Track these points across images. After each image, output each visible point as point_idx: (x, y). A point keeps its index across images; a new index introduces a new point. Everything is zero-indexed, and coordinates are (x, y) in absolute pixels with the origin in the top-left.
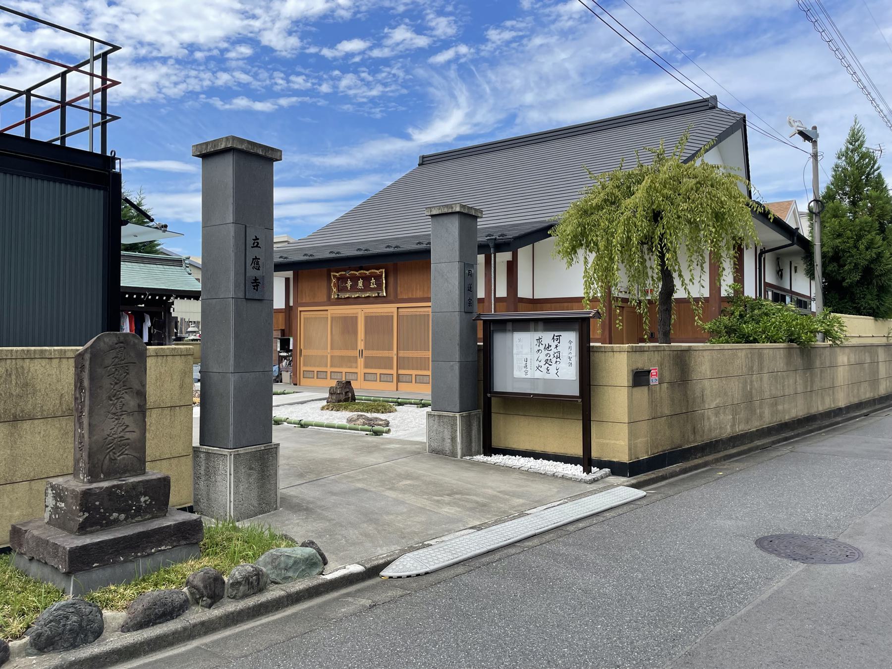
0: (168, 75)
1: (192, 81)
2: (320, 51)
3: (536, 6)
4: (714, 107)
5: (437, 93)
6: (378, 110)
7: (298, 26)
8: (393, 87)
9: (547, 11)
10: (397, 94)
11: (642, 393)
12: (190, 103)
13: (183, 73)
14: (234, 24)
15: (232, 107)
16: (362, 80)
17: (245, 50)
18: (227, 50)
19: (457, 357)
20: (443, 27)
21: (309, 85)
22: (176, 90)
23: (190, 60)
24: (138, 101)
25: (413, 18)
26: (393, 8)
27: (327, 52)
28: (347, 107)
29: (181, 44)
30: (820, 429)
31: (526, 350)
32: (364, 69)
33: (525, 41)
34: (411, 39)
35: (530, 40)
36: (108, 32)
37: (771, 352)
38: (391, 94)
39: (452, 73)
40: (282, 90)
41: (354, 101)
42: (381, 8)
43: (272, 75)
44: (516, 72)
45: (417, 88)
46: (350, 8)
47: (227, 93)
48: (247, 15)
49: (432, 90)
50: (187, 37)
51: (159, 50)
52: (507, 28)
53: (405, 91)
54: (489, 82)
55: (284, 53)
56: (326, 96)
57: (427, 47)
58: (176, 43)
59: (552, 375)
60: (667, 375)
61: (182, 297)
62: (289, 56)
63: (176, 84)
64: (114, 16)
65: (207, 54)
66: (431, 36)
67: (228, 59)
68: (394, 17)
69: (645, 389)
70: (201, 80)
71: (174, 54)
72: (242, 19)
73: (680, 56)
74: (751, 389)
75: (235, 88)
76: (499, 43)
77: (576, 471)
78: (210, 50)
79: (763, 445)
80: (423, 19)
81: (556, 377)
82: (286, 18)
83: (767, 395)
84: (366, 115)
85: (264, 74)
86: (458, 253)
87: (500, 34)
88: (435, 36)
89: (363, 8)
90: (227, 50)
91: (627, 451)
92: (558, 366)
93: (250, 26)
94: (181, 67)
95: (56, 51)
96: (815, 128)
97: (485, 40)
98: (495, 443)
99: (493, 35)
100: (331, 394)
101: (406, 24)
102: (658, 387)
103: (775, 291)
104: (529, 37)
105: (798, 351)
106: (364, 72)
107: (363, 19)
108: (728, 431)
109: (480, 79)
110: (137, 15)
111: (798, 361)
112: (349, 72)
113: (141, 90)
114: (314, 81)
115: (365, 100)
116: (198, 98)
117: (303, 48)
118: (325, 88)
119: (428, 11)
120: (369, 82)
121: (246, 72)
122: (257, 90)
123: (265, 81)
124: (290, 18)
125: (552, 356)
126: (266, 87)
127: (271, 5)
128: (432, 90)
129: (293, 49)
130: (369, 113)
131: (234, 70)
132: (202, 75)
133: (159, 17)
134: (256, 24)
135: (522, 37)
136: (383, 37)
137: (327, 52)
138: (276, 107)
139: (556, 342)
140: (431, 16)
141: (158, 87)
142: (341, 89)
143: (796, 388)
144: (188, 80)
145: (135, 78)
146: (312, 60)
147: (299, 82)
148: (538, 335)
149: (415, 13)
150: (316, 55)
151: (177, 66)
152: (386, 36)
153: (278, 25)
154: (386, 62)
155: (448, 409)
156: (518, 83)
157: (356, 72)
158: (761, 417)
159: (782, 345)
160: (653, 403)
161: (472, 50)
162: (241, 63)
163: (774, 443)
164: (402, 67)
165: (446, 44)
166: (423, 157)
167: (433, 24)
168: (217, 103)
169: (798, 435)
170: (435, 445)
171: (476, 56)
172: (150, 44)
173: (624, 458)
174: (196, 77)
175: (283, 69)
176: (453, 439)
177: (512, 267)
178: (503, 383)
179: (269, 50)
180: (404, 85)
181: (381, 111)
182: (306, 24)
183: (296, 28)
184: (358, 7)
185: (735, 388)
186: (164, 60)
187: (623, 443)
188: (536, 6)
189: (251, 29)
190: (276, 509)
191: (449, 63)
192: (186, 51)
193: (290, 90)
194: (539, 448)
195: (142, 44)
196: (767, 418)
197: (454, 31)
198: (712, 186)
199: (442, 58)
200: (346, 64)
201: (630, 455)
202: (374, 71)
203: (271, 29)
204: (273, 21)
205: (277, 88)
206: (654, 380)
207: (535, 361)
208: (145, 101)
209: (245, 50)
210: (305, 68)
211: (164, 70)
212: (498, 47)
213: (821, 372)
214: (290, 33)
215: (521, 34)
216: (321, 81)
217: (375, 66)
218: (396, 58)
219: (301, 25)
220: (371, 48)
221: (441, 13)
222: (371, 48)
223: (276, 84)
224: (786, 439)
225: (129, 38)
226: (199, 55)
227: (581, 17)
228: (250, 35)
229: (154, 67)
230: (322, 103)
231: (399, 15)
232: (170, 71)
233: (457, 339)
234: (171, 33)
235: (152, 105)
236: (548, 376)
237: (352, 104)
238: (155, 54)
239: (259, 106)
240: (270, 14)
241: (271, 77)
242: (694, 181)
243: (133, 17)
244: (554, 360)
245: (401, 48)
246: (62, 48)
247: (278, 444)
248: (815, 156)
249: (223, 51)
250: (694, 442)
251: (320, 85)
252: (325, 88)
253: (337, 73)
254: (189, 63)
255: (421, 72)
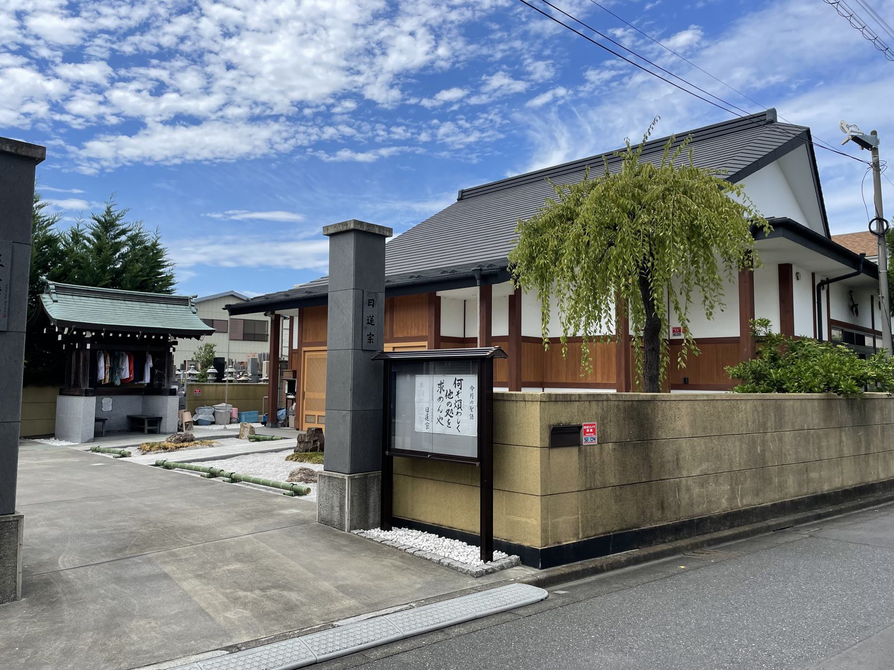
0: (279, 132)
1: (301, 136)
2: (420, 101)
3: (637, 44)
4: (773, 121)
5: (538, 137)
6: (474, 156)
7: (399, 79)
8: (490, 133)
9: (649, 47)
10: (494, 139)
11: (567, 457)
12: (298, 157)
13: (293, 129)
14: (339, 81)
15: (336, 159)
16: (460, 127)
17: (350, 105)
18: (333, 106)
19: (349, 405)
20: (541, 70)
21: (409, 134)
22: (286, 146)
23: (300, 116)
24: (252, 157)
25: (510, 64)
26: (491, 56)
27: (426, 103)
28: (444, 154)
29: (292, 102)
30: (878, 502)
31: (426, 398)
32: (462, 117)
33: (625, 80)
34: (509, 85)
35: (630, 78)
36: (227, 94)
37: (798, 403)
38: (488, 140)
39: (553, 116)
40: (383, 141)
41: (452, 148)
42: (479, 56)
43: (374, 127)
44: (618, 110)
45: (515, 132)
46: (449, 59)
47: (331, 146)
48: (352, 71)
49: (530, 133)
50: (296, 95)
51: (272, 109)
52: (607, 68)
53: (502, 136)
54: (590, 123)
55: (386, 106)
56: (425, 145)
57: (524, 92)
58: (287, 102)
59: (452, 431)
60: (613, 431)
61: (182, 337)
62: (390, 108)
63: (286, 140)
64: (233, 79)
65: (315, 110)
66: (529, 81)
67: (334, 114)
68: (492, 64)
69: (575, 450)
70: (309, 135)
71: (285, 112)
72: (347, 76)
73: (794, 87)
74: (763, 451)
75: (339, 141)
76: (598, 83)
77: (468, 556)
78: (317, 106)
79: (779, 524)
80: (521, 64)
81: (456, 433)
82: (389, 72)
83: (791, 458)
84: (462, 160)
85: (366, 127)
86: (352, 278)
87: (599, 74)
88: (532, 81)
89: (462, 58)
90: (333, 106)
91: (539, 533)
92: (460, 418)
93: (355, 81)
94: (291, 124)
95: (181, 113)
96: (874, 133)
97: (584, 81)
98: (400, 512)
99: (592, 75)
100: (299, 442)
101: (504, 71)
102: (597, 449)
103: (845, 330)
104: (630, 75)
105: (844, 403)
106: (461, 119)
107: (462, 68)
108: (723, 505)
109: (580, 118)
110: (253, 77)
111: (843, 413)
112: (447, 121)
113: (255, 147)
114: (413, 131)
115: (461, 146)
116: (305, 152)
117: (404, 100)
118: (424, 137)
119: (526, 56)
120: (467, 129)
121: (351, 126)
122: (360, 142)
123: (367, 133)
124: (392, 72)
125: (453, 406)
126: (368, 139)
127: (375, 60)
128: (530, 133)
129: (394, 101)
130: (466, 159)
131: (339, 124)
132: (310, 130)
133: (272, 78)
134: (360, 79)
135: (623, 75)
136: (481, 85)
137: (426, 103)
138: (377, 157)
139: (458, 388)
140: (529, 61)
141: (270, 143)
142: (439, 137)
143: (841, 450)
144: (297, 136)
145: (250, 136)
146: (412, 111)
147: (399, 132)
148: (437, 379)
149: (513, 59)
150: (416, 106)
151: (288, 123)
152: (484, 83)
153: (381, 78)
154: (483, 108)
155: (339, 470)
156: (620, 122)
157: (454, 120)
158: (781, 486)
159: (816, 395)
160: (587, 469)
161: (570, 92)
162: (345, 117)
163: (797, 522)
164: (500, 112)
165: (544, 87)
166: (462, 192)
167: (530, 69)
168: (323, 156)
169: (840, 512)
170: (324, 513)
171: (575, 98)
172: (264, 104)
173: (535, 542)
174: (304, 133)
175: (384, 121)
176: (342, 507)
177: (515, 303)
178: (403, 441)
179: (371, 103)
180: (501, 129)
181: (477, 157)
182: (407, 77)
183: (397, 81)
184: (457, 57)
185: (735, 452)
186: (276, 118)
187: (535, 523)
188: (637, 44)
189: (355, 84)
190: (15, 599)
191: (547, 106)
192: (296, 109)
193: (390, 141)
194: (445, 522)
195: (256, 103)
196: (792, 488)
197: (552, 75)
198: (685, 193)
199: (539, 101)
200: (445, 113)
201: (545, 538)
202: (471, 119)
203: (374, 84)
204: (376, 76)
205: (379, 139)
206: (589, 439)
207: (438, 412)
208: (258, 156)
209: (350, 105)
210: (405, 118)
211: (276, 127)
212: (597, 88)
213: (883, 430)
214: (392, 86)
215: (621, 72)
216: (420, 130)
217: (472, 112)
218: (493, 104)
219: (402, 79)
220: (469, 96)
221: (538, 57)
222: (469, 96)
223: (378, 135)
224: (819, 517)
225: (246, 99)
226: (307, 112)
227: (685, 52)
228: (354, 90)
229: (267, 124)
230: (420, 151)
231: (496, 62)
232: (282, 128)
233: (350, 383)
234: (282, 92)
235: (265, 160)
236: (449, 431)
237: (450, 151)
238: (268, 112)
239: (361, 157)
240: (374, 69)
241: (373, 129)
242: (662, 187)
243: (250, 80)
244: (455, 410)
245: (498, 94)
246: (186, 110)
247: (22, 517)
248: (876, 166)
249: (330, 107)
250: (661, 520)
251: (419, 134)
252: (424, 137)
253: (435, 121)
254: (298, 119)
255: (517, 116)
